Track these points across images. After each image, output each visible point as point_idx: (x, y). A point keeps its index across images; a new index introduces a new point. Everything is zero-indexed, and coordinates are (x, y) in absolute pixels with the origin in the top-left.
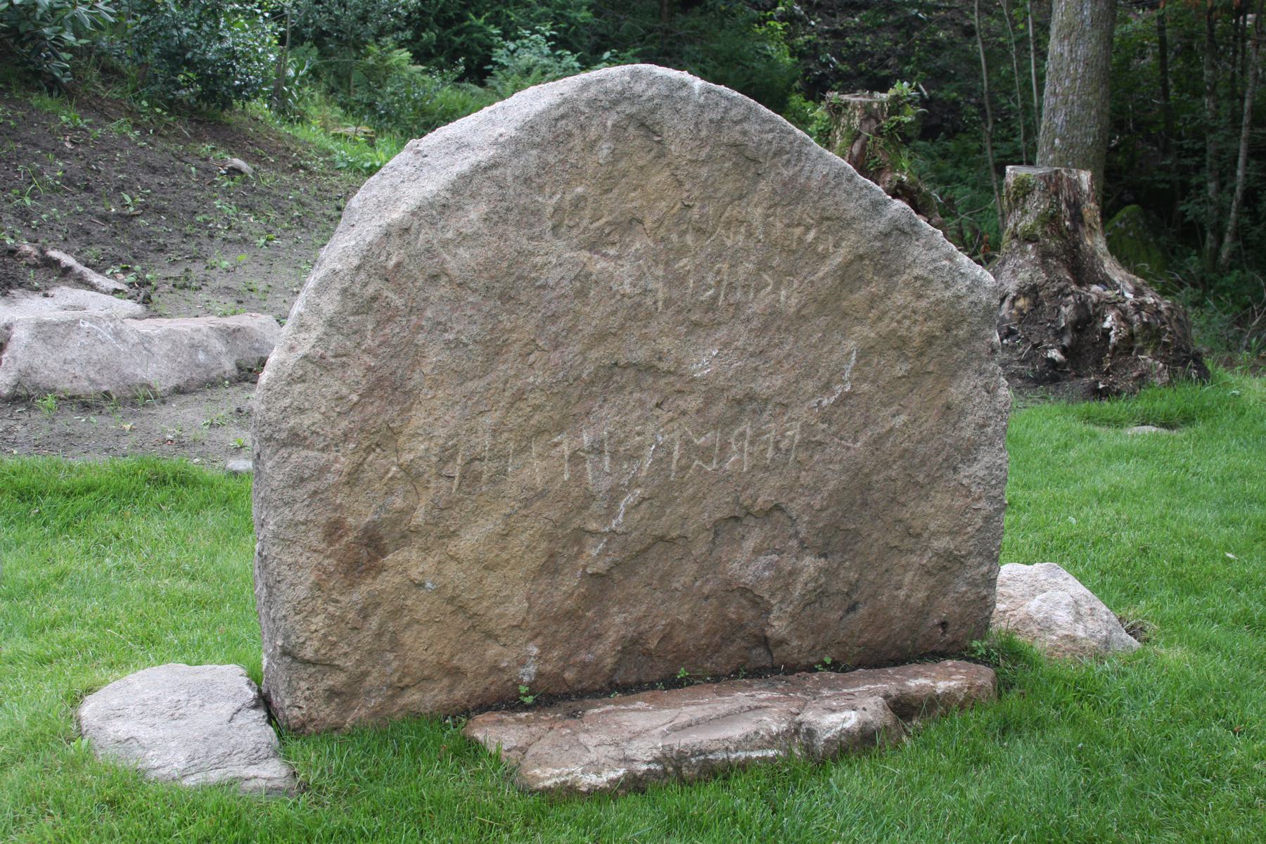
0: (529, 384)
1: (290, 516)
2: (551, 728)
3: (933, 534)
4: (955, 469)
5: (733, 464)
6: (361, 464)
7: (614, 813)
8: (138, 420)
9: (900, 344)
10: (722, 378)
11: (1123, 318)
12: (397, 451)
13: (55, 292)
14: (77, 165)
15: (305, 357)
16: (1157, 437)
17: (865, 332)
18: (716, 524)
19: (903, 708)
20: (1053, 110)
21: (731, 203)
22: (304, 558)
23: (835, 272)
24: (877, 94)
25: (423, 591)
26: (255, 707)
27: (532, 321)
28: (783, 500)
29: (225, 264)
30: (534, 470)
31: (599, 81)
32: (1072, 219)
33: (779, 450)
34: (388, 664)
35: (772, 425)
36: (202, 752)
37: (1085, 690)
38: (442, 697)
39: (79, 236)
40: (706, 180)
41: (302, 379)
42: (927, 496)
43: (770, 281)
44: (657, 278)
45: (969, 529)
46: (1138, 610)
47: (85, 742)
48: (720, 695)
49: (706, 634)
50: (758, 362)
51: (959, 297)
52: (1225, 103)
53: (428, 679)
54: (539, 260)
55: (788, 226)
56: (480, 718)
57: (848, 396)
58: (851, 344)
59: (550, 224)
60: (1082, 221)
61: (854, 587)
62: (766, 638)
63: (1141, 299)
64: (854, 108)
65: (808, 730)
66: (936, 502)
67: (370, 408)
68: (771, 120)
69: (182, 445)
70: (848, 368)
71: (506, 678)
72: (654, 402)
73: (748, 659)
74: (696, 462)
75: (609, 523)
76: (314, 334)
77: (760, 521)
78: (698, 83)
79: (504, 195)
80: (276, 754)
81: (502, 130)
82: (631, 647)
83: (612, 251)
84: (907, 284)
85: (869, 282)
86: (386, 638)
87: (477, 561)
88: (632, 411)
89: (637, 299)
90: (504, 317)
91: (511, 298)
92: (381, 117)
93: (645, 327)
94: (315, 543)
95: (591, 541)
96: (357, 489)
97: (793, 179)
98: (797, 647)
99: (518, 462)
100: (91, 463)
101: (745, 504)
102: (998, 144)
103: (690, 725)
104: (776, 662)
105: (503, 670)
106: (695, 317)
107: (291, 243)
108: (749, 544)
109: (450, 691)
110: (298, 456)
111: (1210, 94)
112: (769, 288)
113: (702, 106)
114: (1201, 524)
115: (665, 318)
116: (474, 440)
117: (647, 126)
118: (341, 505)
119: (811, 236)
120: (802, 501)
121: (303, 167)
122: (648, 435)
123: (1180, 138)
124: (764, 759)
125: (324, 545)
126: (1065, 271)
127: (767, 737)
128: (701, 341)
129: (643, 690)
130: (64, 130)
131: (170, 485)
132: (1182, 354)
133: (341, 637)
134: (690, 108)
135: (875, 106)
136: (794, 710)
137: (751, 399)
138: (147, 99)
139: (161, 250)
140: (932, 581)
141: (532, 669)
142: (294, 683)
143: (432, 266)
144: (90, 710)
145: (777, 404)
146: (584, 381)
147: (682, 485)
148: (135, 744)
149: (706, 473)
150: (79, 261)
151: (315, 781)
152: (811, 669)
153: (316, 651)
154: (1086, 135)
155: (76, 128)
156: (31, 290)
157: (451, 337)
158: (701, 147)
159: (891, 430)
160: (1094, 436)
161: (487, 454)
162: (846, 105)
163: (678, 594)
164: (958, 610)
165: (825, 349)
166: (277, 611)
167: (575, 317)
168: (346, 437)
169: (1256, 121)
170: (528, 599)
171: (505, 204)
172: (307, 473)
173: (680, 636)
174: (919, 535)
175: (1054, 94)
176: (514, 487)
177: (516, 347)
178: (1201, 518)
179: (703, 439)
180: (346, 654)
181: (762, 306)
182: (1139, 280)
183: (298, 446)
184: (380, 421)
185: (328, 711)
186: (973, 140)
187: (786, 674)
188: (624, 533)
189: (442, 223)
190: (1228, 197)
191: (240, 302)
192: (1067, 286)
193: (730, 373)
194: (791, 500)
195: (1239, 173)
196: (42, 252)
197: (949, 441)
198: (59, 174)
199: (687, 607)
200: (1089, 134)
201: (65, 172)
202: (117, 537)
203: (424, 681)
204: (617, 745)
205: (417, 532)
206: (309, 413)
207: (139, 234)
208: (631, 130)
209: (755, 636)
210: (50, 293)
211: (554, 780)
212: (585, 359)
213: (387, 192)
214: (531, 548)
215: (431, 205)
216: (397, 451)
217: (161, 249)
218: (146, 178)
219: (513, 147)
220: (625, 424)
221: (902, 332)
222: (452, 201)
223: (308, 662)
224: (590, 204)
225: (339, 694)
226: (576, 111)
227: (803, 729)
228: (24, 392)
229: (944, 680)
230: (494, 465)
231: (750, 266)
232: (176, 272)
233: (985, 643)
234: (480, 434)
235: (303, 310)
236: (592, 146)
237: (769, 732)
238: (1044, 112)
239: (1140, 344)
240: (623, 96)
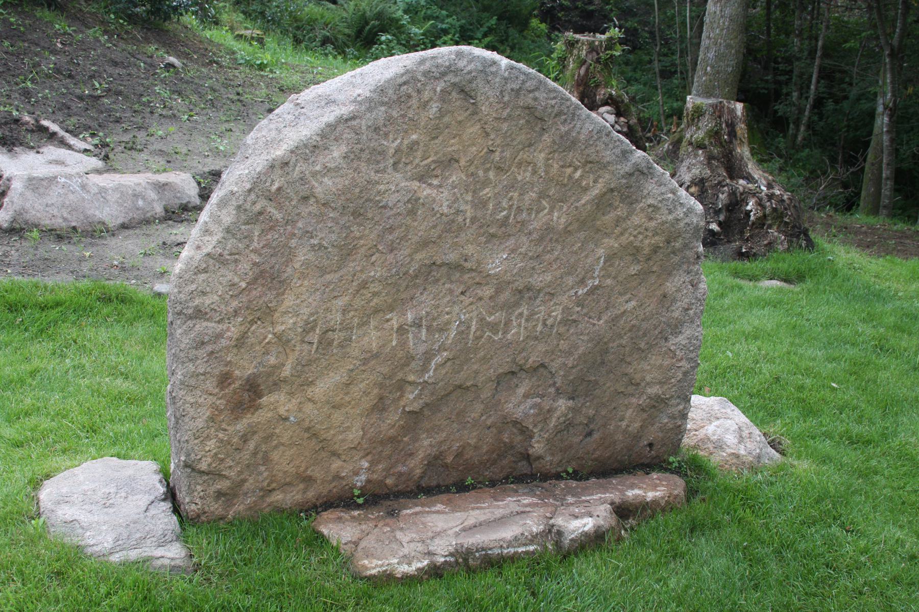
1: (193, 369)
2: (376, 526)
3: (648, 384)
4: (666, 339)
5: (513, 335)
6: (246, 333)
7: (420, 594)
8: (95, 249)
9: (634, 252)
10: (509, 274)
11: (760, 204)
12: (273, 323)
13: (44, 150)
14: (64, 59)
15: (208, 254)
16: (780, 290)
18: (499, 377)
19: (622, 511)
20: (708, 48)
21: (523, 149)
22: (202, 399)
23: (593, 200)
24: (598, 35)
25: (288, 423)
26: (164, 500)
27: (375, 232)
29: (160, 133)
30: (372, 338)
31: (433, 58)
32: (729, 135)
33: (546, 325)
34: (261, 474)
35: (542, 308)
36: (125, 536)
37: (746, 497)
38: (299, 497)
39: (63, 110)
40: (506, 132)
41: (205, 271)
44: (467, 202)
45: (673, 380)
46: (776, 428)
47: (42, 520)
48: (496, 500)
49: (487, 452)
50: (534, 263)
51: (678, 220)
52: (807, 42)
53: (289, 484)
55: (562, 167)
56: (325, 515)
57: (596, 288)
58: (601, 252)
59: (391, 161)
60: (735, 136)
61: (591, 420)
62: (528, 455)
63: (771, 191)
64: (583, 44)
65: (558, 531)
66: (652, 362)
67: (254, 292)
68: (555, 90)
69: (124, 269)
70: (598, 269)
71: (344, 483)
72: (460, 290)
73: (515, 469)
75: (423, 376)
78: (504, 62)
80: (178, 539)
81: (360, 91)
82: (434, 462)
83: (435, 182)
84: (642, 210)
85: (616, 208)
86: (260, 456)
87: (328, 402)
89: (452, 217)
90: (355, 228)
91: (360, 214)
92: (268, 21)
93: (457, 237)
94: (211, 389)
95: (409, 388)
96: (242, 350)
97: (568, 133)
98: (550, 462)
99: (360, 332)
100: (60, 283)
102: (661, 58)
103: (475, 526)
104: (534, 471)
105: (343, 478)
107: (205, 118)
108: (521, 391)
109: (304, 492)
110: (201, 326)
111: (797, 36)
112: (546, 211)
113: (506, 79)
114: (814, 359)
115: (471, 231)
117: (465, 92)
118: (230, 361)
119: (578, 174)
121: (215, 62)
122: (454, 314)
123: (776, 62)
124: (527, 553)
125: (217, 390)
126: (723, 169)
127: (529, 537)
128: (495, 247)
129: (441, 493)
130: (57, 35)
131: (113, 303)
132: (796, 230)
133: (228, 455)
134: (497, 80)
135: (597, 43)
136: (548, 515)
138: (114, 13)
139: (118, 122)
140: (645, 415)
141: (363, 478)
142: (192, 486)
143: (304, 190)
144: (47, 494)
146: (410, 275)
148: (77, 525)
149: (494, 341)
150: (62, 128)
151: (205, 563)
152: (558, 477)
153: (209, 465)
154: (728, 66)
155: (65, 33)
156: (28, 148)
158: (503, 108)
159: (625, 312)
160: (741, 288)
161: (338, 327)
162: (577, 42)
163: (469, 425)
164: (660, 435)
165: (583, 255)
166: (181, 436)
168: (236, 313)
169: (825, 55)
170: (363, 429)
171: (359, 146)
172: (207, 339)
173: (469, 454)
174: (638, 384)
175: (709, 38)
176: (357, 351)
178: (813, 354)
179: (493, 317)
180: (230, 467)
181: (540, 224)
182: (770, 178)
183: (200, 319)
185: (216, 506)
186: (646, 54)
187: (541, 480)
190: (805, 102)
191: (169, 162)
192: (724, 180)
193: (515, 271)
194: (552, 361)
195: (812, 87)
196: (37, 121)
197: (663, 319)
198: (52, 66)
199: (475, 434)
200: (730, 66)
201: (55, 64)
202: (75, 342)
203: (286, 485)
204: (423, 542)
205: (285, 381)
206: (210, 295)
207: (103, 109)
208: (454, 94)
209: (521, 454)
210: (41, 150)
211: (378, 569)
212: (412, 260)
213: (273, 134)
214: (366, 393)
215: (305, 146)
216: (273, 323)
217: (118, 121)
218: (110, 69)
219: (368, 105)
220: (438, 307)
221: (637, 244)
222: (321, 143)
223: (203, 472)
225: (224, 495)
226: (415, 79)
227: (555, 530)
228: (18, 226)
229: (650, 490)
230: (342, 335)
231: (534, 195)
232: (126, 138)
233: (679, 459)
234: (334, 312)
235: (207, 220)
236: (425, 105)
237: (531, 533)
238: (702, 49)
239: (770, 222)
240: (450, 70)
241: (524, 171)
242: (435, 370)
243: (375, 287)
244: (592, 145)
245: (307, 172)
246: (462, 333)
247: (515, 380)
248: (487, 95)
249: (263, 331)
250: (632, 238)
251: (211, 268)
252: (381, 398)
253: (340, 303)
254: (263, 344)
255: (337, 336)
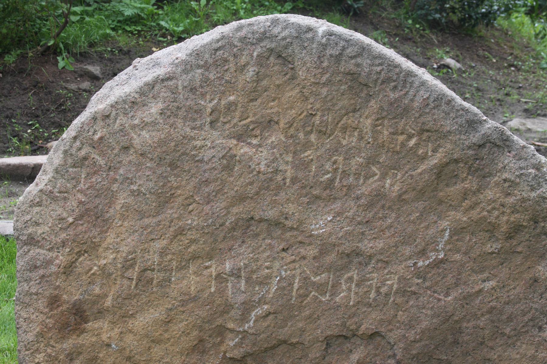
0: (188, 225)
1: (27, 288)
15: (41, 191)
17: (460, 216)
21: (347, 114)
22: (35, 316)
23: (431, 170)
28: (383, 330)
30: (190, 281)
35: (375, 275)
40: (326, 97)
41: (39, 204)
42: (514, 344)
43: (377, 172)
44: (287, 163)
54: (198, 143)
55: (393, 134)
57: (442, 261)
58: (445, 224)
59: (208, 120)
67: (80, 228)
72: (281, 247)
74: (313, 293)
76: (49, 176)
77: (365, 342)
79: (175, 98)
83: (255, 142)
84: (497, 184)
87: (147, 336)
88: (264, 251)
93: (276, 195)
94: (42, 308)
95: (230, 335)
96: (71, 278)
101: (351, 328)
106: (316, 192)
110: (35, 251)
116: (147, 256)
118: (59, 286)
119: (412, 142)
120: (399, 332)
122: (275, 269)
125: (47, 310)
128: (320, 209)
134: (314, 46)
137: (357, 254)
145: (378, 261)
147: (301, 308)
149: (321, 301)
157: (135, 188)
158: (322, 74)
159: (480, 291)
167: (221, 183)
168: (64, 244)
172: (39, 263)
176: (175, 292)
177: (180, 199)
179: (318, 278)
181: (369, 189)
183: (35, 246)
184: (86, 237)
188: (253, 334)
189: (132, 113)
194: (391, 331)
197: (535, 306)
206: (42, 226)
212: (229, 213)
215: (125, 102)
219: (183, 67)
220: (257, 260)
221: (492, 219)
224: (240, 109)
230: (161, 275)
234: (151, 253)
236: (242, 69)
240: (264, 36)
241: (350, 136)
242: (255, 321)
243: (192, 235)
244: (428, 113)
245: (127, 125)
246: (285, 288)
247: (349, 345)
248: (305, 63)
249: (89, 263)
250: (485, 213)
251: (44, 202)
252: (201, 341)
253: (158, 246)
254: (89, 275)
255: (157, 276)
